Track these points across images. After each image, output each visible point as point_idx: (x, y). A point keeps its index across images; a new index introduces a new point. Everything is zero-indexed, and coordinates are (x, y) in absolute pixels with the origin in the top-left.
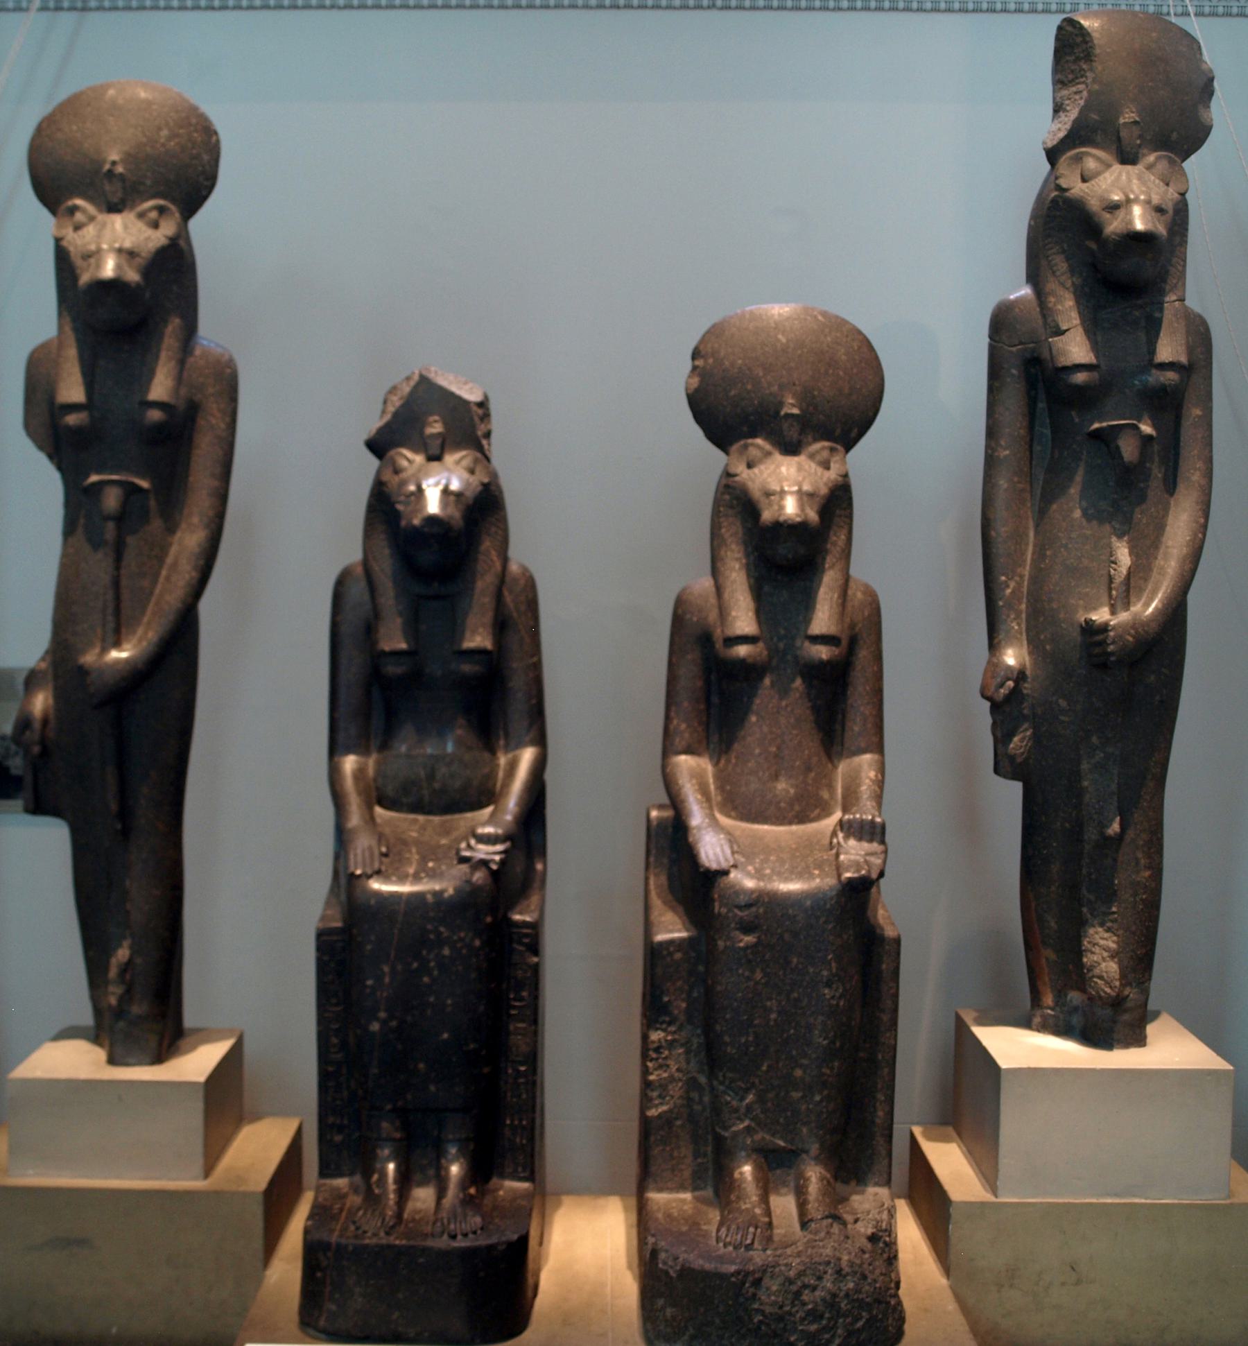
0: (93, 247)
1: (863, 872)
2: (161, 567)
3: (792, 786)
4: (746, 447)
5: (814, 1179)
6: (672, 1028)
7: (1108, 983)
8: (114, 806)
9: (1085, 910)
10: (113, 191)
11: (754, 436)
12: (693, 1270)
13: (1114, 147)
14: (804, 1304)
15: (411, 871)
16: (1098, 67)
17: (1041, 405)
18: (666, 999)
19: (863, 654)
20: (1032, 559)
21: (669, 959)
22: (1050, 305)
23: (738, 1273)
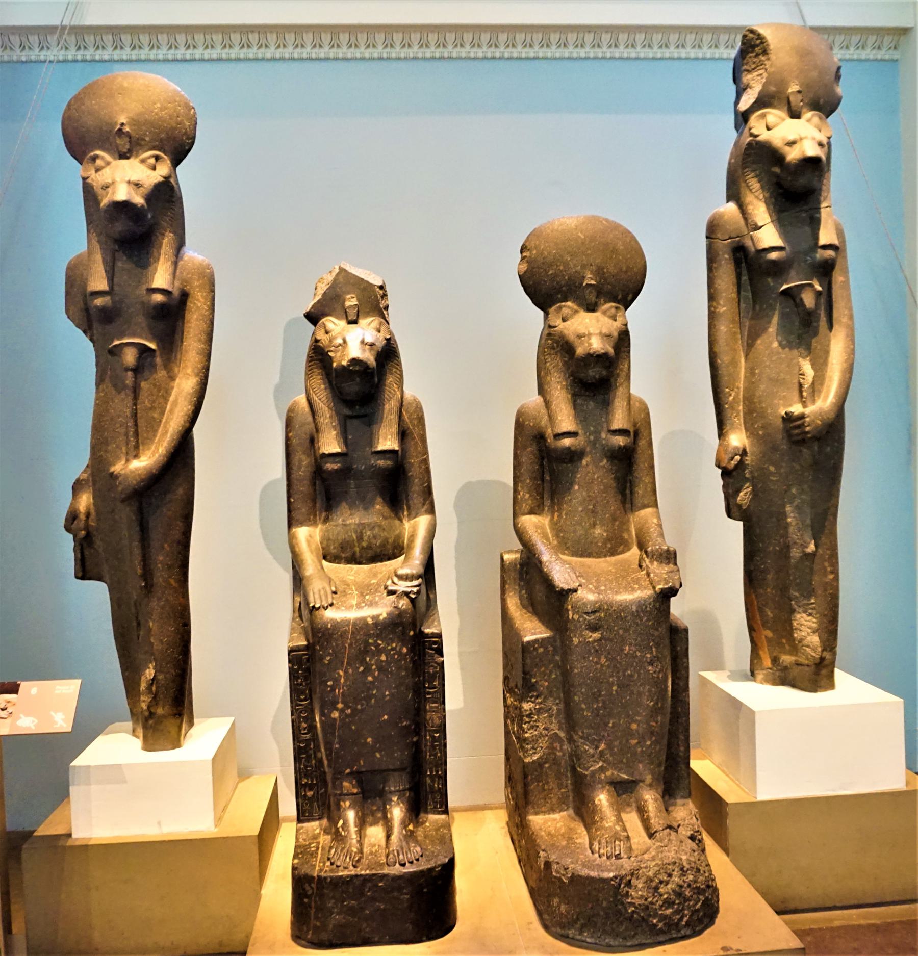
0: (110, 181)
1: (670, 584)
2: (166, 403)
3: (605, 531)
4: (560, 308)
5: (650, 801)
6: (539, 700)
7: (814, 650)
8: (139, 571)
9: (793, 602)
10: (123, 144)
11: (566, 301)
12: (581, 877)
13: (786, 108)
14: (661, 895)
15: (354, 602)
16: (772, 56)
17: (745, 278)
18: (534, 680)
19: (642, 443)
20: (745, 377)
21: (535, 653)
22: (750, 211)
23: (615, 877)
